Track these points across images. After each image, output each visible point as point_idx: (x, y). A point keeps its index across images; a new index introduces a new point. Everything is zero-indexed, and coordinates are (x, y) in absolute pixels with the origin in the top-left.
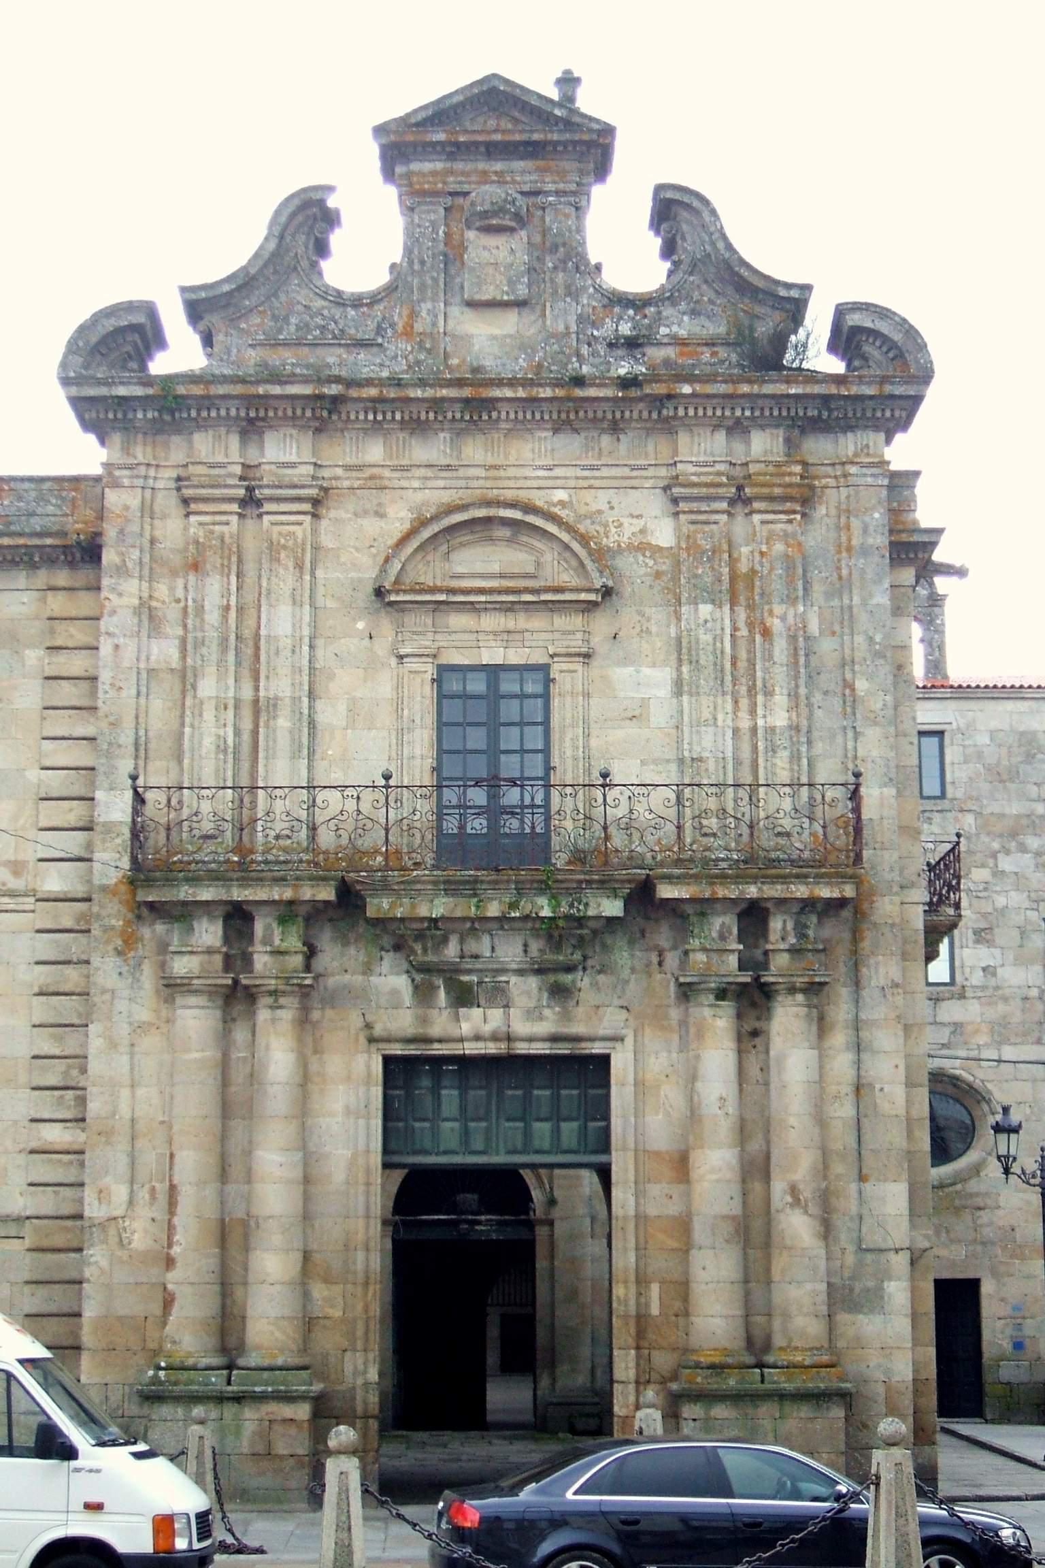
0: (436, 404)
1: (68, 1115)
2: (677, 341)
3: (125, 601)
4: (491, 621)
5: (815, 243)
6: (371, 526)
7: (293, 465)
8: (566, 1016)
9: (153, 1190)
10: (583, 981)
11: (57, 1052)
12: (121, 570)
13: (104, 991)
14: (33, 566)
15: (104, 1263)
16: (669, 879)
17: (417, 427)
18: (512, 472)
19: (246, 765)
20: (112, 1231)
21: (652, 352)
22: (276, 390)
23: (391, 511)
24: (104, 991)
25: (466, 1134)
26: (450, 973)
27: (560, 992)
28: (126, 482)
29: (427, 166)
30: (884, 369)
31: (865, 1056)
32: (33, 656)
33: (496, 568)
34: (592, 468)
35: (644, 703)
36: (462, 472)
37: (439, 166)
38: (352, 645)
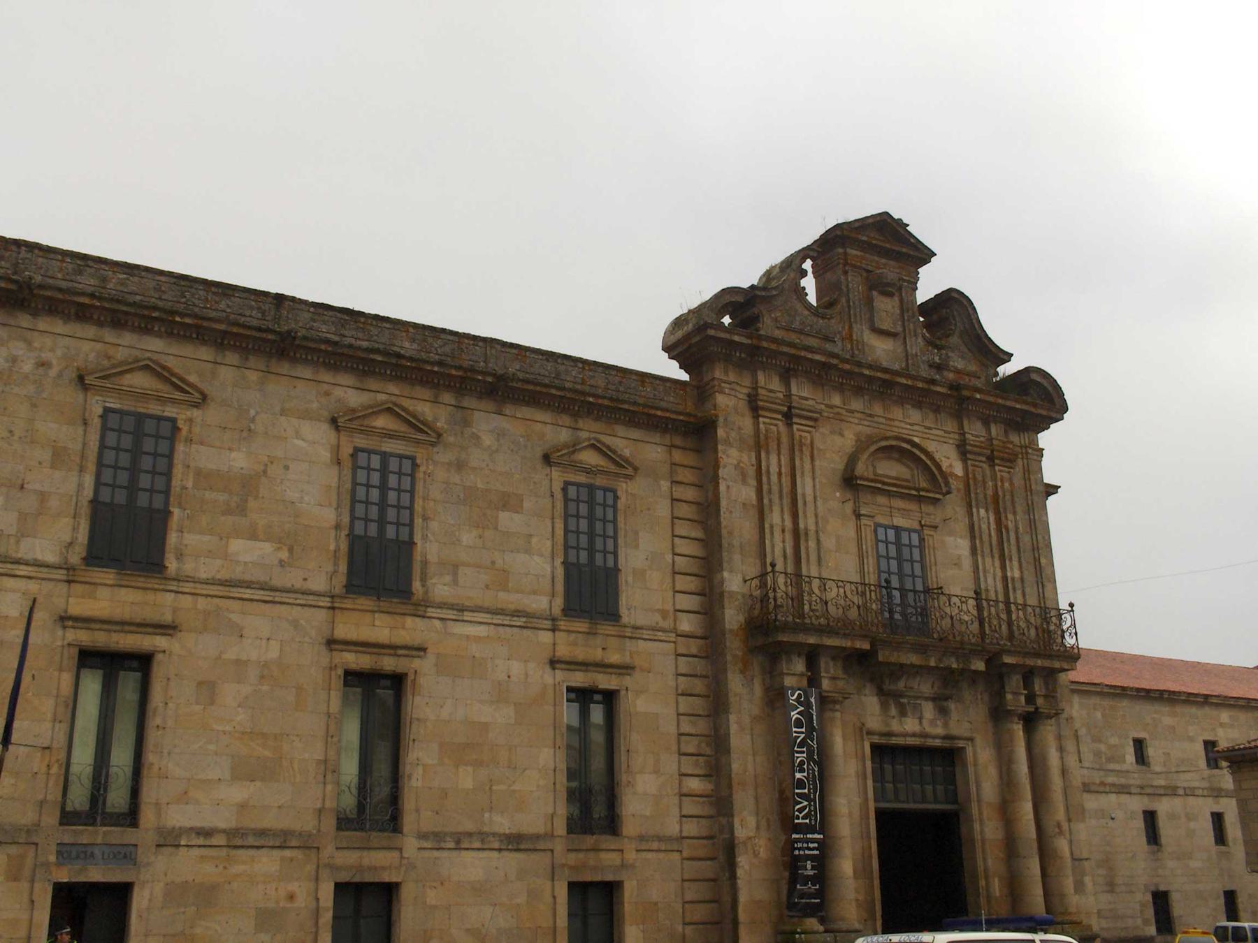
0: (871, 379)
1: (701, 772)
2: (958, 371)
3: (730, 461)
4: (898, 503)
5: (1021, 335)
6: (838, 440)
7: (806, 399)
8: (946, 725)
9: (768, 820)
10: (952, 705)
11: (693, 731)
12: (727, 442)
13: (736, 695)
14: (665, 431)
15: (747, 867)
16: (1009, 652)
17: (859, 391)
18: (896, 423)
19: (311, 600)
20: (749, 847)
21: (946, 373)
22: (810, 356)
23: (846, 433)
24: (736, 695)
25: (896, 791)
26: (897, 695)
27: (943, 712)
28: (727, 391)
29: (854, 252)
30: (1039, 399)
31: (1065, 754)
32: (665, 485)
33: (894, 474)
34: (930, 428)
35: (959, 557)
36: (876, 419)
37: (859, 253)
38: (834, 504)
